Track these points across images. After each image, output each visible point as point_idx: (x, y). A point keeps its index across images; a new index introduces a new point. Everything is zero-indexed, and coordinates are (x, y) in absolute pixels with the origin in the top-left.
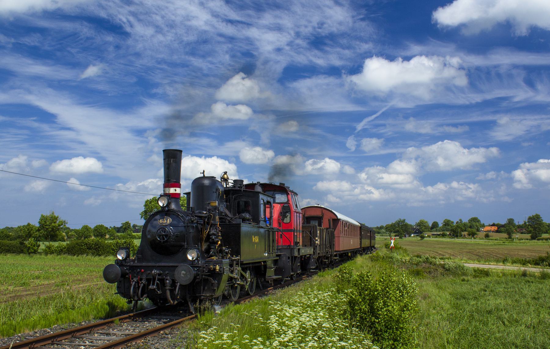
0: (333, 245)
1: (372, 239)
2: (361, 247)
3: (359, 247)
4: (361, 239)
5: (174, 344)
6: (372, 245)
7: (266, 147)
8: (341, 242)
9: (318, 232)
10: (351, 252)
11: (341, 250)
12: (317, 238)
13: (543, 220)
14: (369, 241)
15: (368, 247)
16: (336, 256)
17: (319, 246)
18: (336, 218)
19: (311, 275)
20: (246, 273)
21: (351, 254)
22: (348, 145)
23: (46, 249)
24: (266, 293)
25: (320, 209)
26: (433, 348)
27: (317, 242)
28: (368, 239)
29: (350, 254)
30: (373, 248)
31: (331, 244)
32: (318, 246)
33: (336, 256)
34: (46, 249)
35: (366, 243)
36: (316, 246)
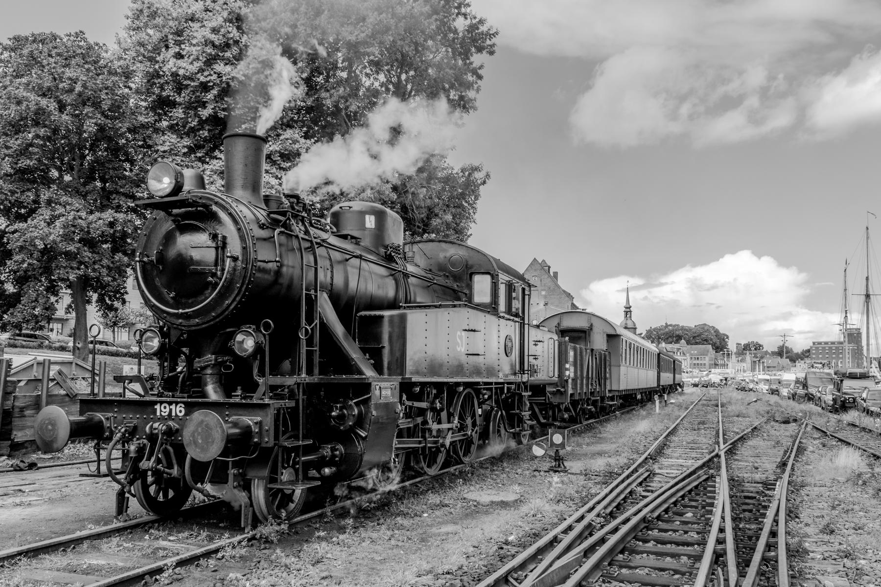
0: (605, 378)
1: (676, 372)
2: (659, 385)
4: (659, 373)
8: (622, 373)
10: (641, 393)
11: (622, 388)
13: (334, 193)
16: (612, 399)
17: (573, 380)
18: (613, 333)
19: (778, 566)
20: (232, 468)
23: (375, 100)
25: (586, 316)
27: (567, 373)
29: (639, 397)
31: (602, 376)
32: (570, 381)
33: (612, 399)
34: (375, 100)
35: (667, 378)
36: (567, 381)
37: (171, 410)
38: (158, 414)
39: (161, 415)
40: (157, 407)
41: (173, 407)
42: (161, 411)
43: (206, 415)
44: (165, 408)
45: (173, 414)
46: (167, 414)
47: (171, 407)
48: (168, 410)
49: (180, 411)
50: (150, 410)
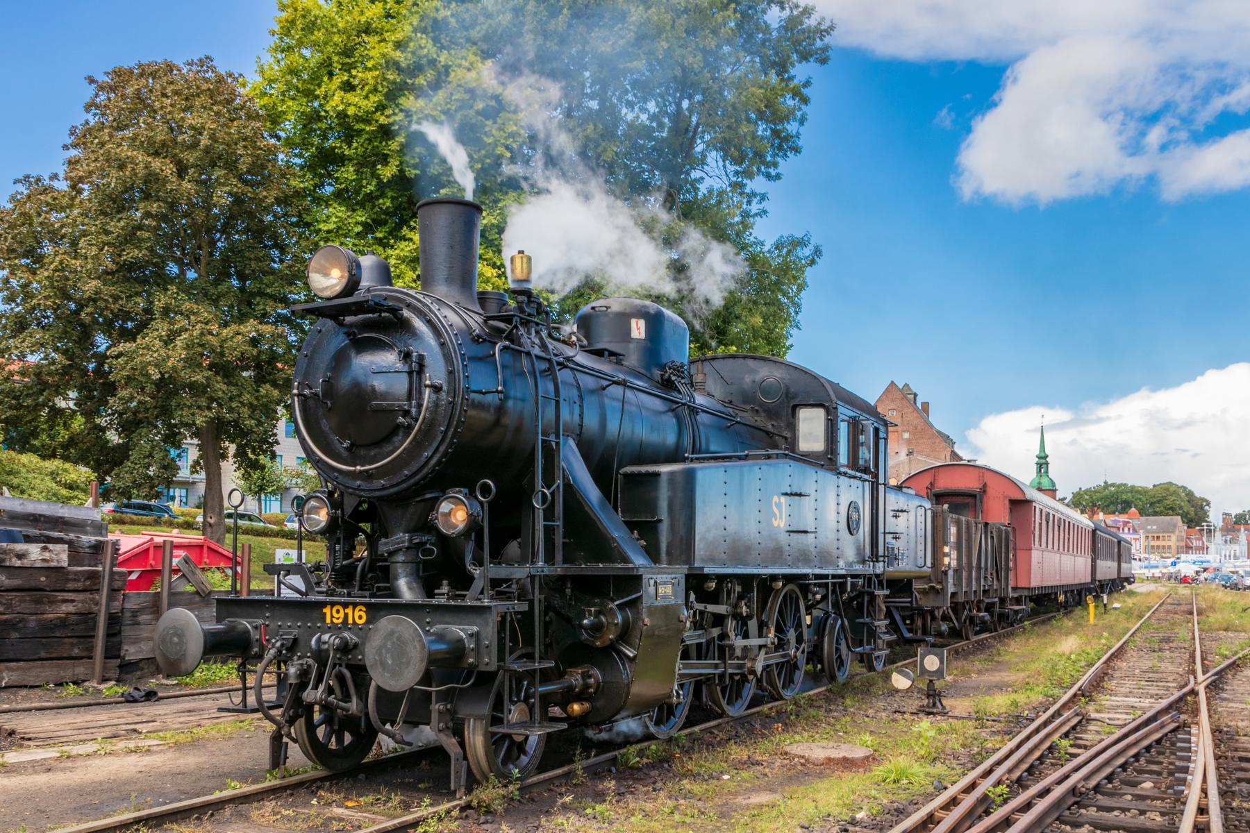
1: (1123, 558)
2: (1093, 580)
3: (1089, 580)
4: (1094, 561)
5: (384, 40)
6: (1122, 576)
7: (818, 49)
9: (953, 530)
10: (1065, 593)
12: (946, 549)
14: (1115, 565)
15: (1113, 581)
16: (1018, 601)
21: (1066, 596)
22: (446, 511)
24: (101, 320)
26: (2, 346)
27: (946, 560)
28: (1113, 561)
30: (1125, 584)
31: (1000, 567)
32: (951, 573)
33: (1018, 601)
35: (1107, 568)
36: (945, 573)
37: (346, 615)
38: (328, 621)
39: (332, 621)
40: (327, 610)
41: (349, 611)
42: (332, 617)
43: (399, 622)
44: (338, 611)
45: (350, 621)
46: (340, 620)
47: (347, 611)
48: (342, 614)
49: (360, 617)
50: (316, 614)
